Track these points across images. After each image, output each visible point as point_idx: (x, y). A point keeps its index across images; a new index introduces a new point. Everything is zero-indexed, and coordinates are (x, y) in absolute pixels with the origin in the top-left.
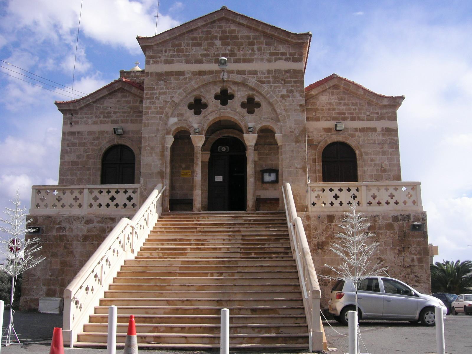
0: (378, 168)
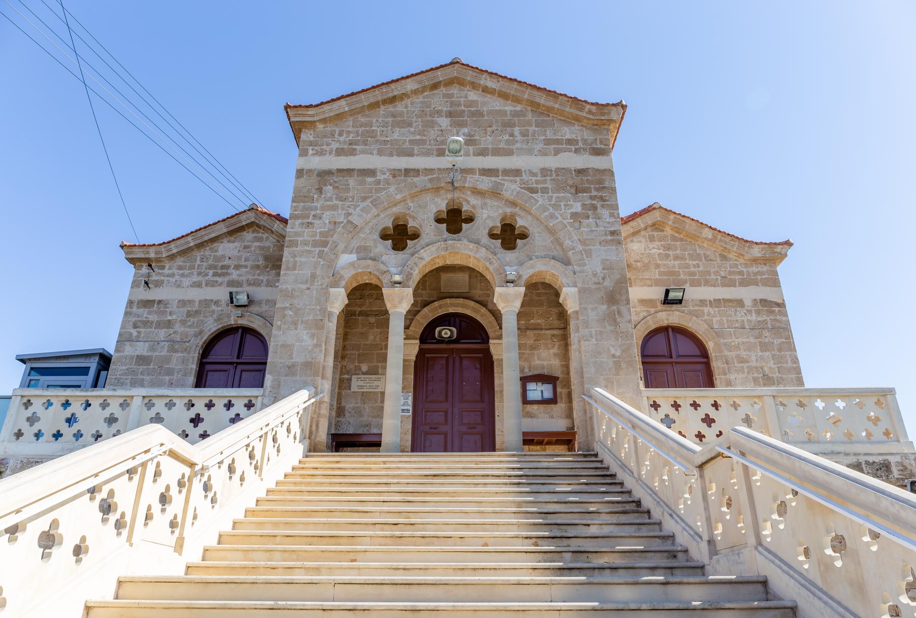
0: (756, 375)
